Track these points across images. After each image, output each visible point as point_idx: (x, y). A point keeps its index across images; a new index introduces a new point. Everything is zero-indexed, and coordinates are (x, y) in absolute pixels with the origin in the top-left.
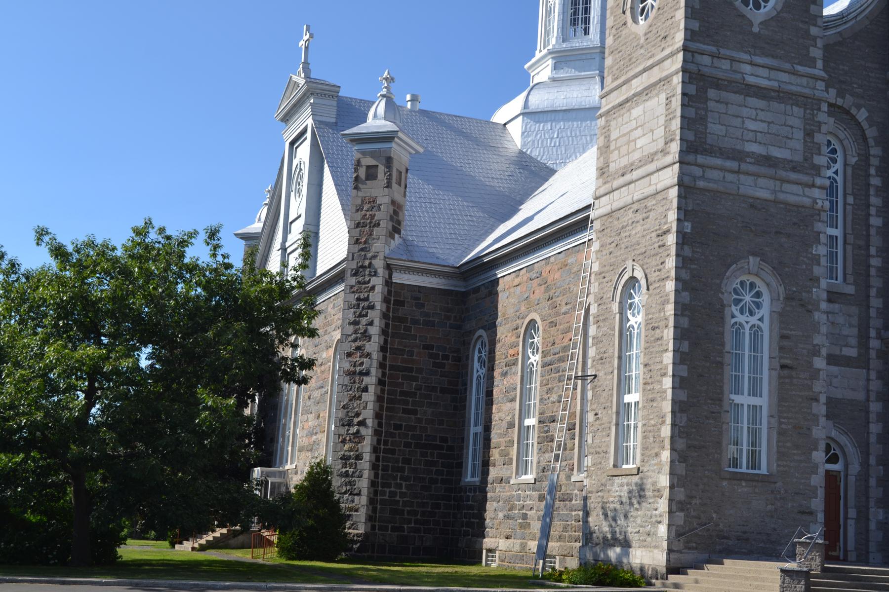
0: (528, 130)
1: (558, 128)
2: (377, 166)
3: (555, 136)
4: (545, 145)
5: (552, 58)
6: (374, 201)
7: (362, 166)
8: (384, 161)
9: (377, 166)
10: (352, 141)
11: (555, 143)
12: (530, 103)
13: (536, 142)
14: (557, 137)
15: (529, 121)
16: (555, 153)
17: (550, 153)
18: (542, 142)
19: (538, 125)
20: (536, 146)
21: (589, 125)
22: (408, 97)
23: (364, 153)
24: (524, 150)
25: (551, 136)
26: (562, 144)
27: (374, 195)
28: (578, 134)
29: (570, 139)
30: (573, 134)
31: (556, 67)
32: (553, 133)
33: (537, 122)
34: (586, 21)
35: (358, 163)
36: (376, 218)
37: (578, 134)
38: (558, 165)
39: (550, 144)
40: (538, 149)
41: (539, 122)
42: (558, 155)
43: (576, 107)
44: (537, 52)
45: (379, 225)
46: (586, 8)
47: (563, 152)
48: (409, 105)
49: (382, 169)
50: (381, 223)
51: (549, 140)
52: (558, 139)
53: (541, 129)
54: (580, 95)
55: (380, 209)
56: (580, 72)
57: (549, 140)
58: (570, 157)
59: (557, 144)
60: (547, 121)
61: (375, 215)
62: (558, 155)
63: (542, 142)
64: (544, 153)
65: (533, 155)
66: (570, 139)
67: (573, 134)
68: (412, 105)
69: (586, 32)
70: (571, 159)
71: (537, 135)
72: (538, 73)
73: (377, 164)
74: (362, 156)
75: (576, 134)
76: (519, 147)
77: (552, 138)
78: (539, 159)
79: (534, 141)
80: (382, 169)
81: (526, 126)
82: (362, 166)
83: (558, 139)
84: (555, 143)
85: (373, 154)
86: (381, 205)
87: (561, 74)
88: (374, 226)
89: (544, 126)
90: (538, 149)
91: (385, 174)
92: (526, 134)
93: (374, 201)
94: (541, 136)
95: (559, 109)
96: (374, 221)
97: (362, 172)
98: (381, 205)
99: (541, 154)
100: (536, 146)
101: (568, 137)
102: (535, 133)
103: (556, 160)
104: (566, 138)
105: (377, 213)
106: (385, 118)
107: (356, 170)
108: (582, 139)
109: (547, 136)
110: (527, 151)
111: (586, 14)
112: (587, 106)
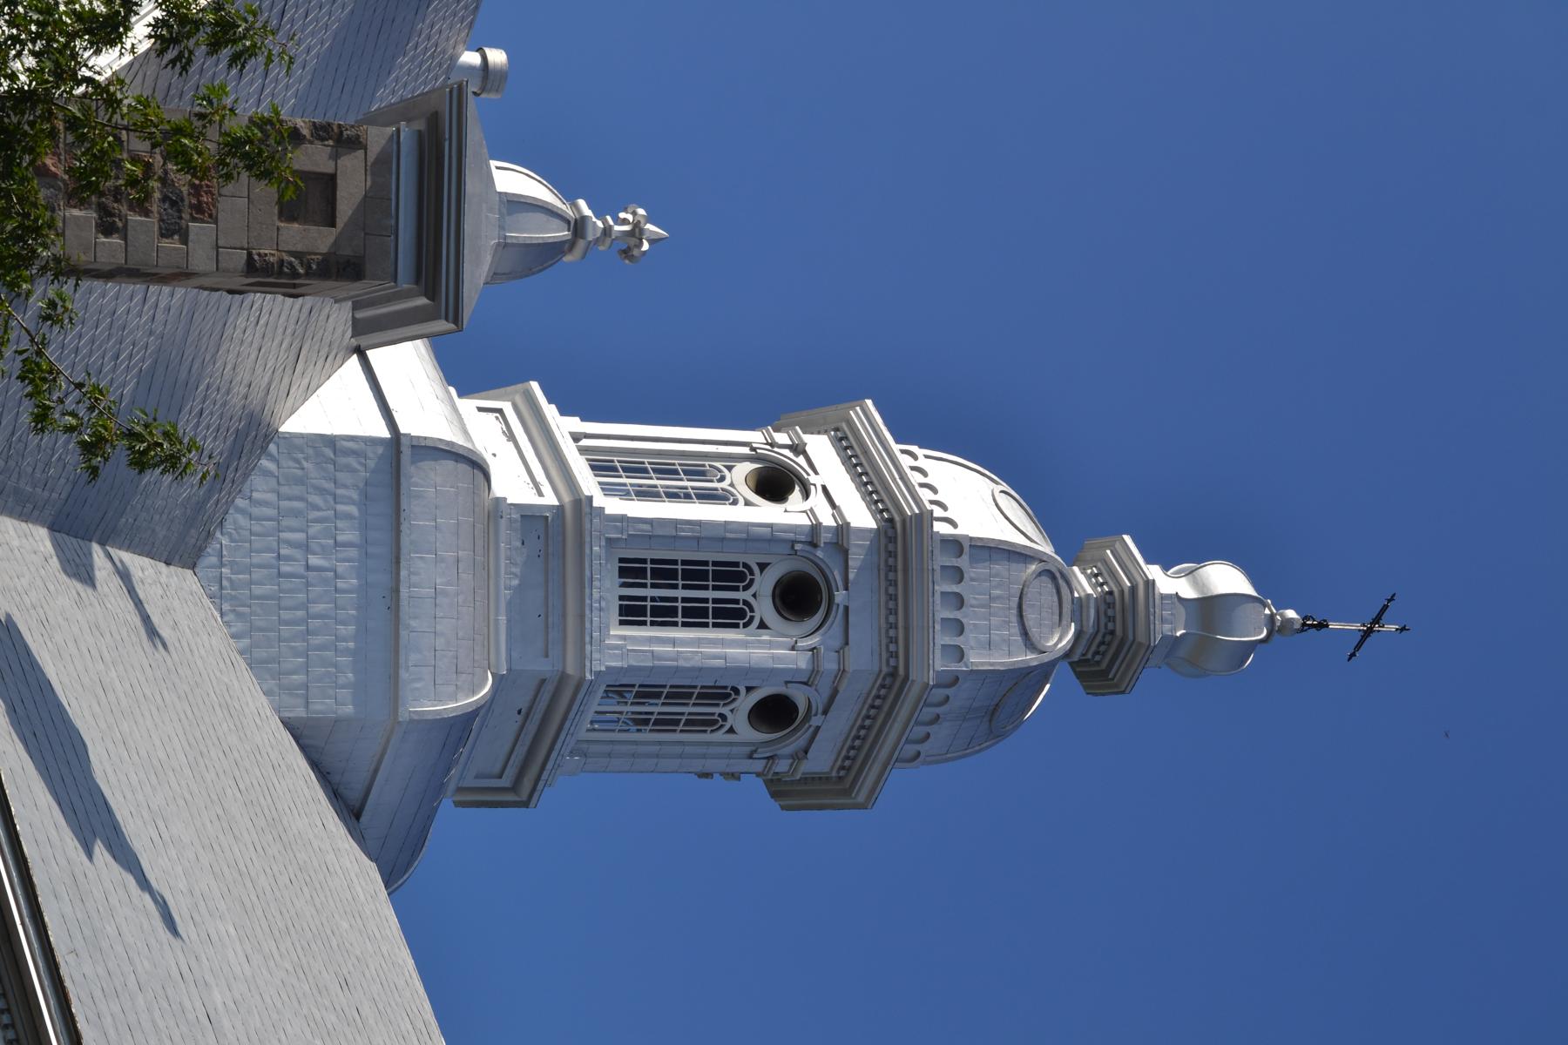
0: (342, 460)
1: (342, 567)
2: (332, 223)
3: (314, 560)
4: (285, 522)
5: (560, 509)
6: (199, 208)
7: (335, 157)
8: (347, 251)
9: (332, 223)
10: (434, 120)
11: (289, 559)
12: (427, 465)
13: (297, 490)
14: (308, 568)
15: (371, 464)
16: (256, 559)
17: (258, 543)
18: (296, 514)
19: (355, 495)
20: (285, 490)
21: (342, 680)
22: (497, 57)
23: (383, 166)
24: (272, 448)
25: (314, 545)
26: (286, 584)
27: (224, 205)
28: (316, 640)
29: (300, 613)
30: (315, 623)
31: (529, 517)
32: (324, 552)
33: (365, 496)
34: (663, 614)
35: (346, 142)
36: (134, 218)
37: (316, 640)
38: (214, 573)
39: (290, 543)
40: (271, 497)
41: (366, 499)
42: (248, 569)
43: (403, 633)
44: (575, 424)
45: (107, 229)
46: (703, 613)
47: (257, 590)
48: (471, 58)
49: (320, 240)
50: (116, 240)
51: (300, 536)
52: (302, 570)
53: (340, 507)
54: (440, 642)
55: (166, 233)
56: (509, 603)
57: (300, 536)
58: (240, 615)
59: (285, 568)
60: (364, 527)
61: (147, 213)
62: (248, 569)
63: (296, 514)
64: (258, 519)
65: (256, 480)
66: (300, 613)
67: (315, 623)
68: (470, 69)
69: (631, 613)
70: (231, 617)
71: (322, 491)
72: (511, 437)
73: (340, 222)
74: (372, 157)
75: (315, 633)
76: (282, 429)
77: (306, 548)
78: (239, 502)
79: (300, 481)
80: (320, 240)
81: (354, 453)
82: (335, 157)
83: (302, 570)
84: (289, 559)
85: (377, 201)
86: (185, 241)
87: (507, 539)
88: (104, 211)
89: (349, 516)
90: (271, 497)
91: (292, 253)
92: (329, 452)
93: (199, 208)
94: (317, 508)
95: (403, 573)
96: (124, 209)
97: (313, 158)
98: (185, 241)
99: (256, 511)
100: (285, 490)
101: (304, 606)
102: (329, 486)
103: (232, 564)
104: (302, 596)
105: (153, 221)
106: (505, 246)
107: (322, 132)
108: (297, 655)
109: (315, 528)
110: (272, 458)
111: (687, 612)
112: (404, 675)
